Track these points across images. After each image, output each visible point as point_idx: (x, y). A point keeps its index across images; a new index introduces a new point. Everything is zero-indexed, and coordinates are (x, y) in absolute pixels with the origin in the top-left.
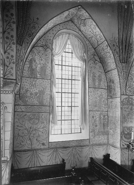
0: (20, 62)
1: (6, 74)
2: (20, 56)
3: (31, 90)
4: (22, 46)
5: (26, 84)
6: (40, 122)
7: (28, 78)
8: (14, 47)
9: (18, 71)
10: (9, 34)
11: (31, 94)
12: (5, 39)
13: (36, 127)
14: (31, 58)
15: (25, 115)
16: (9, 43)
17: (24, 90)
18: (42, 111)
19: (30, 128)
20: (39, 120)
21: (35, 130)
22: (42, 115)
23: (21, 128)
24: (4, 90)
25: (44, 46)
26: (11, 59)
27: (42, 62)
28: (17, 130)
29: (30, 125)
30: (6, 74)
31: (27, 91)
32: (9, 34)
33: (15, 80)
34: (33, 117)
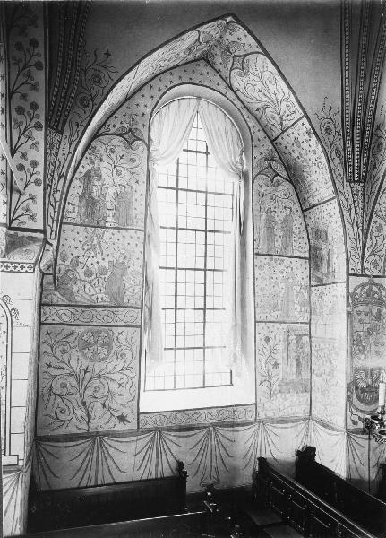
1: (16, 216)
4: (61, 133)
8: (39, 136)
10: (26, 100)
11: (88, 273)
14: (88, 167)
16: (24, 125)
17: (68, 263)
19: (86, 372)
20: (108, 345)
22: (120, 334)
26: (29, 170)
29: (85, 363)
30: (16, 216)
31: (76, 262)
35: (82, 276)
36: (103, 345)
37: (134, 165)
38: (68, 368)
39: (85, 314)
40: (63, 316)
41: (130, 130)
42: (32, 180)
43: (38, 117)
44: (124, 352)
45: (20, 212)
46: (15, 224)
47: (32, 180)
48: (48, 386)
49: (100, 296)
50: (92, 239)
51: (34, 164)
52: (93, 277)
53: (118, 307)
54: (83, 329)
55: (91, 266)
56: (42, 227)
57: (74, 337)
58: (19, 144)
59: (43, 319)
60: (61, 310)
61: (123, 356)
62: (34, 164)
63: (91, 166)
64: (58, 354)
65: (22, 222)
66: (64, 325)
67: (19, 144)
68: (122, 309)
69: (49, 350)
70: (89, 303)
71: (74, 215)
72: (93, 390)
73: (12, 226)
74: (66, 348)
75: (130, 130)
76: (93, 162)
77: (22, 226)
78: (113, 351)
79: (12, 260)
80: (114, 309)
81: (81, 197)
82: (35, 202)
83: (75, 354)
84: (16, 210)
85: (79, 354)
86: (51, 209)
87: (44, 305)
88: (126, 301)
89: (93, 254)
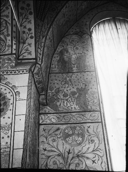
0: (42, 38)
1: (21, 54)
2: (42, 32)
3: (65, 90)
4: (43, 21)
5: (56, 81)
6: (85, 140)
7: (59, 73)
8: (32, 18)
9: (40, 48)
10: (26, 29)
11: (65, 95)
12: (20, 11)
13: (80, 151)
14: (61, 49)
15: (58, 129)
16: (24, 14)
17: (53, 91)
18: (87, 121)
19: (69, 153)
20: (83, 136)
21: (78, 156)
22: (89, 127)
23: (51, 154)
24: (17, 70)
25: (78, 33)
26: (26, 9)
27: (77, 51)
28: (44, 156)
29: (68, 147)
30: (21, 54)
31: (58, 91)
32: (26, 29)
33: (33, 59)
34: (71, 132)
35: (62, 97)
36: (78, 135)
37: (85, 44)
38: (58, 151)
39: (65, 117)
40: (53, 120)
41: (80, 31)
42: (29, 37)
43: (30, 9)
44: (93, 138)
45: (23, 51)
46: (21, 57)
47: (29, 37)
48: (45, 164)
49: (73, 107)
50: (66, 79)
51: (30, 30)
52: (68, 97)
53: (85, 112)
54: (64, 126)
55: (66, 92)
56: (34, 57)
57: (60, 131)
58: (22, 23)
59: (41, 122)
60: (51, 116)
61: (93, 141)
62: (30, 30)
63: (62, 48)
64: (51, 143)
65: (24, 56)
66: (52, 124)
67: (22, 23)
68: (87, 113)
69: (45, 140)
70: (67, 111)
71: (55, 69)
72: (75, 165)
73: (20, 58)
74: (55, 138)
75: (80, 31)
76: (63, 47)
77: (24, 58)
78: (85, 139)
79: (18, 69)
80: (83, 113)
81: (58, 61)
82: (31, 46)
83: (61, 142)
84: (23, 24)
85: (64, 142)
86: (39, 50)
87: (41, 114)
88: (89, 107)
89: (67, 86)
